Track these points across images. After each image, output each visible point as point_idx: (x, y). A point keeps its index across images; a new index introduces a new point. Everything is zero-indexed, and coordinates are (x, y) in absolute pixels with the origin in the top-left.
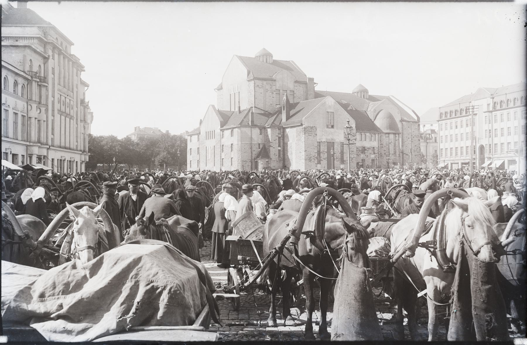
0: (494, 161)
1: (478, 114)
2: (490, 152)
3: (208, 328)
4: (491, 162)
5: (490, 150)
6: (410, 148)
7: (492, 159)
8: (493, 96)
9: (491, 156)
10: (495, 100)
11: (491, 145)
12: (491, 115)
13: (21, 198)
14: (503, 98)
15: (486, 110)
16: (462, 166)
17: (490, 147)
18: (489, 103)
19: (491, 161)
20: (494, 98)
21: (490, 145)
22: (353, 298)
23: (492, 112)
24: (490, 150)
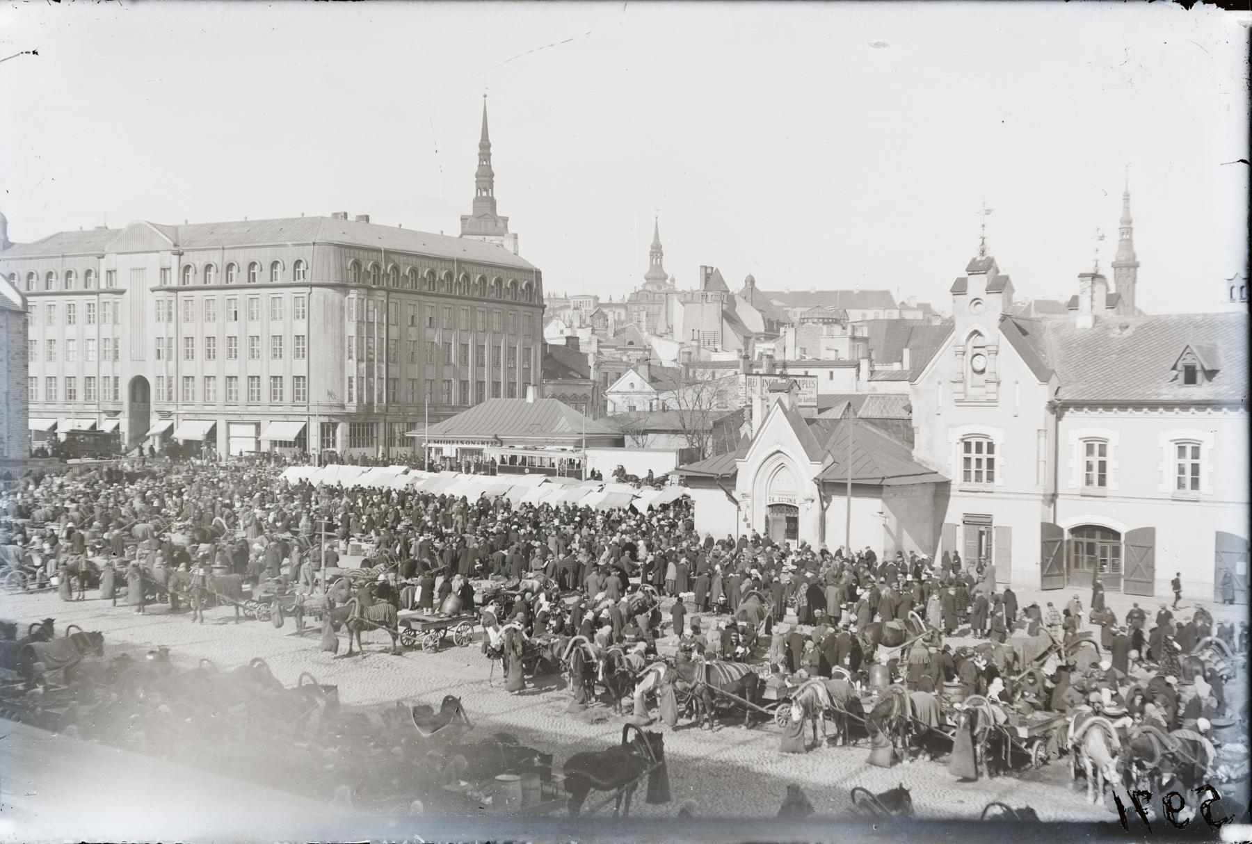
0: (180, 421)
1: (127, 295)
2: (170, 398)
3: (190, 559)
4: (172, 426)
5: (170, 393)
6: (5, 390)
7: (173, 417)
8: (181, 249)
9: (173, 409)
10: (185, 260)
11: (174, 341)
12: (174, 299)
13: (881, 796)
14: (216, 258)
15: (157, 284)
16: (167, 572)
17: (170, 386)
18: (166, 265)
19: (169, 423)
20: (182, 254)
21: (170, 339)
22: (893, 768)
23: (176, 290)
24: (170, 393)
